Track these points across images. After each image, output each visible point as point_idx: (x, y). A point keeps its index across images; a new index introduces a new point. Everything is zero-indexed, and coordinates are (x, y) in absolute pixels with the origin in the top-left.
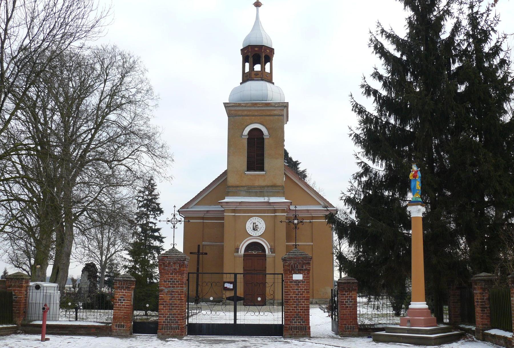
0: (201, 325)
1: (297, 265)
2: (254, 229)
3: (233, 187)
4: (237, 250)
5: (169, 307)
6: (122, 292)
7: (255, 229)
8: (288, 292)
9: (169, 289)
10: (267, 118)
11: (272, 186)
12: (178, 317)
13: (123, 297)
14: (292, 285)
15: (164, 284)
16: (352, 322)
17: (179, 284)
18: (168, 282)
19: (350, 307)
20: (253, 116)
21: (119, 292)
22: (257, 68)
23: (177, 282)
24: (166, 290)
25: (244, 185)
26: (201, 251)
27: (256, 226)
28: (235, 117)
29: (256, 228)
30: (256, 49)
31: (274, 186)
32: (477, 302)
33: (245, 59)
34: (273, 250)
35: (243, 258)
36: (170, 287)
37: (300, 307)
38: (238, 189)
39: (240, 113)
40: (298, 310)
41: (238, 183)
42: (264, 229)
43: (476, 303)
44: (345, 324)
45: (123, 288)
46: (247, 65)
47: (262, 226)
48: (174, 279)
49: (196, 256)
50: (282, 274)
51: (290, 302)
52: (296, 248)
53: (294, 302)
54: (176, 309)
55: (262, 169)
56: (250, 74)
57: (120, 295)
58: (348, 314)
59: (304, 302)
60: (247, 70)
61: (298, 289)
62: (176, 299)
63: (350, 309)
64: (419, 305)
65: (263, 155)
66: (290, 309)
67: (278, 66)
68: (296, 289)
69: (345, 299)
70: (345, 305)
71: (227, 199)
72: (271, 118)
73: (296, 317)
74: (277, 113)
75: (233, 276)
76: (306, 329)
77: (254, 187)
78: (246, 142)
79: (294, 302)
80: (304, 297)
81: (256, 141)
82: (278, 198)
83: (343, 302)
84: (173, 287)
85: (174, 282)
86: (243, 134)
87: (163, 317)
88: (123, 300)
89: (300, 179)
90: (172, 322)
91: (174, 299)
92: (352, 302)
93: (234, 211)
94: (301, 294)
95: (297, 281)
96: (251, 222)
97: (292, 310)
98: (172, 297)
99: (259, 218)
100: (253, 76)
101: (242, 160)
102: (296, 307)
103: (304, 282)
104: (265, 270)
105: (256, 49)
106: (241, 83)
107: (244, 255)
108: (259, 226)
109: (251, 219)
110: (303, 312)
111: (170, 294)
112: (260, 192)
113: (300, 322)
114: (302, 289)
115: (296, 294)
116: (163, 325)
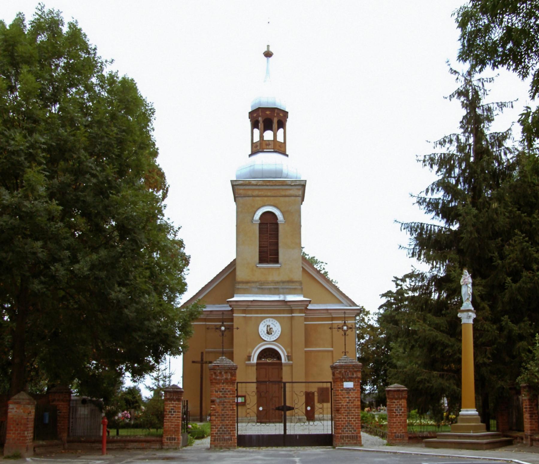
0: (250, 436)
2: (268, 333)
3: (243, 282)
4: (249, 358)
6: (173, 404)
7: (269, 333)
8: (339, 400)
10: (282, 199)
13: (173, 409)
16: (402, 430)
17: (230, 394)
18: (220, 392)
19: (400, 415)
20: (266, 196)
21: (169, 404)
22: (268, 135)
23: (229, 391)
25: (256, 280)
26: (204, 360)
27: (270, 329)
29: (270, 332)
30: (268, 112)
31: (291, 282)
32: (526, 408)
33: (255, 125)
34: (289, 358)
35: (255, 367)
36: (221, 397)
39: (250, 193)
41: (248, 278)
42: (280, 333)
43: (524, 410)
44: (396, 433)
46: (257, 132)
47: (277, 328)
48: (227, 389)
49: (199, 365)
50: (331, 382)
52: (345, 355)
54: (228, 420)
55: (276, 261)
57: (170, 407)
59: (355, 410)
60: (257, 139)
61: (349, 398)
62: (228, 410)
64: (469, 411)
65: (277, 244)
66: (341, 418)
67: (293, 132)
68: (347, 398)
70: (395, 413)
71: (235, 299)
73: (347, 426)
74: (293, 191)
76: (357, 438)
77: (267, 283)
79: (345, 410)
80: (355, 405)
81: (269, 228)
82: (295, 295)
84: (225, 397)
85: (226, 392)
86: (254, 218)
87: (216, 428)
88: (174, 412)
90: (225, 434)
93: (244, 311)
95: (348, 390)
96: (264, 324)
97: (344, 418)
98: (224, 407)
99: (274, 320)
105: (268, 112)
106: (250, 156)
107: (257, 363)
108: (274, 329)
109: (265, 320)
110: (354, 421)
112: (275, 288)
116: (215, 436)
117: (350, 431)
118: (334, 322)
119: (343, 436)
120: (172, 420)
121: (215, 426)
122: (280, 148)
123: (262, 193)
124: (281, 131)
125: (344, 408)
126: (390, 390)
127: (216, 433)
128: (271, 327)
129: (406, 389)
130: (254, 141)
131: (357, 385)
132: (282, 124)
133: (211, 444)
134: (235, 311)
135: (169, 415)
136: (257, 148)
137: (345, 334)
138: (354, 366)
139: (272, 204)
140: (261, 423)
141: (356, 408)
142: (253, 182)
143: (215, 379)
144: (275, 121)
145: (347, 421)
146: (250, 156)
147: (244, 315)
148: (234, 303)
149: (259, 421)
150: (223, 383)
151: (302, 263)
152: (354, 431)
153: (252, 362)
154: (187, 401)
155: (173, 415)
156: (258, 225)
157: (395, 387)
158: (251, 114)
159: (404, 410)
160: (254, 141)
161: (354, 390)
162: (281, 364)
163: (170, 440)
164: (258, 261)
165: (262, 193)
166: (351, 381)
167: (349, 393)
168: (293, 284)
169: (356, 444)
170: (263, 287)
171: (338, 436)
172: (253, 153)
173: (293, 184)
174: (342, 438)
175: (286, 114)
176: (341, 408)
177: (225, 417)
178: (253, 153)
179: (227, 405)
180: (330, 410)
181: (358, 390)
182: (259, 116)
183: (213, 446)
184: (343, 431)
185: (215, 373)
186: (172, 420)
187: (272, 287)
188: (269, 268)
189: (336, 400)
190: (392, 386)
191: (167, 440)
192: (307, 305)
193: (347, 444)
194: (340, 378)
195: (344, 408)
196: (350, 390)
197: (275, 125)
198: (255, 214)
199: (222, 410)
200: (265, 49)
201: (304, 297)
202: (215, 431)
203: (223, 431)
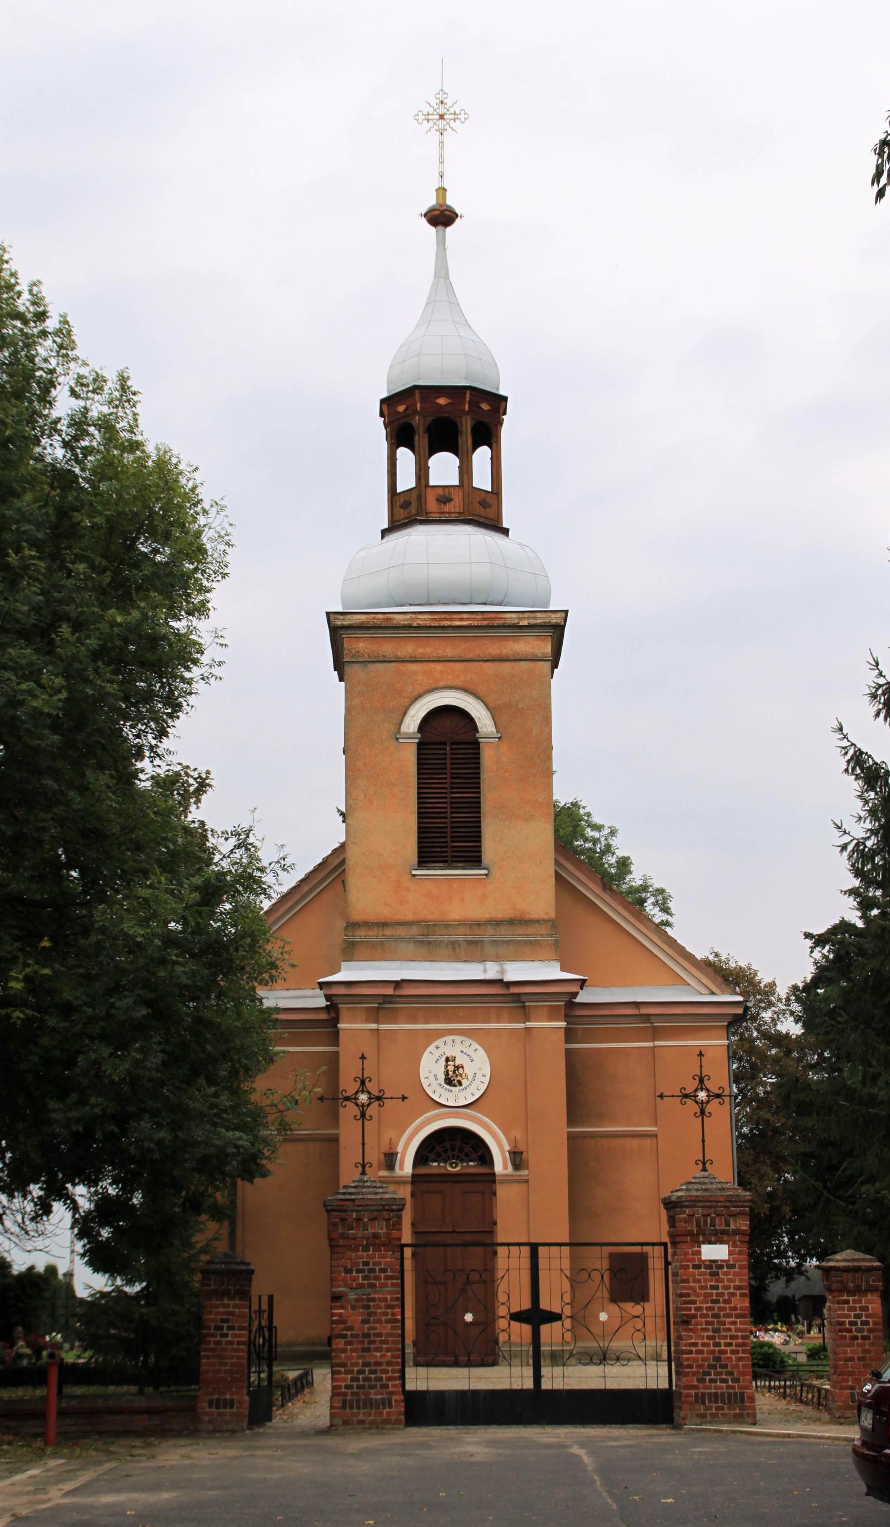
1: (713, 1219)
2: (449, 1081)
3: (368, 925)
4: (390, 1159)
5: (362, 1342)
6: (225, 1306)
8: (688, 1295)
9: (359, 1291)
11: (512, 922)
12: (387, 1372)
14: (701, 1274)
15: (345, 1279)
17: (387, 1278)
18: (358, 1271)
19: (863, 1338)
21: (217, 1306)
22: (444, 468)
23: (383, 1270)
24: (352, 1296)
25: (410, 917)
27: (457, 1068)
28: (372, 667)
29: (455, 1076)
30: (442, 401)
33: (400, 434)
34: (517, 1158)
36: (361, 1286)
37: (725, 1337)
38: (388, 932)
40: (719, 1345)
41: (384, 912)
42: (487, 1080)
44: (852, 1388)
45: (226, 1294)
47: (478, 1067)
48: (375, 1264)
50: (665, 1245)
51: (697, 1324)
53: (707, 1323)
54: (379, 1350)
56: (419, 498)
58: (859, 1359)
59: (734, 1323)
60: (406, 481)
61: (717, 1288)
62: (380, 1321)
63: (862, 1345)
65: (475, 806)
66: (695, 1344)
68: (712, 1287)
69: (849, 1316)
70: (850, 1331)
72: (506, 667)
73: (714, 1367)
75: (526, 1250)
76: (743, 1401)
77: (447, 925)
78: (409, 756)
79: (707, 1323)
80: (735, 1308)
83: (843, 1323)
84: (372, 1286)
85: (373, 1271)
86: (404, 729)
87: (346, 1372)
89: (628, 906)
90: (371, 1387)
91: (375, 1322)
92: (867, 1323)
93: (375, 1015)
94: (725, 1302)
95: (714, 1265)
97: (704, 1345)
98: (370, 1314)
99: (468, 1041)
100: (432, 505)
101: (397, 826)
102: (713, 1338)
103: (733, 1266)
104: (491, 1233)
105: (442, 401)
106: (384, 533)
107: (416, 1179)
108: (469, 1070)
110: (732, 1352)
111: (364, 1307)
112: (470, 943)
113: (726, 1381)
114: (728, 1288)
115: (713, 1301)
116: (345, 1394)
117: (723, 1381)
118: (657, 1043)
119: (703, 1394)
120: (226, 1350)
121: (344, 1365)
122: (482, 511)
123: (428, 650)
124: (482, 456)
125: (703, 1316)
126: (831, 1267)
127: (347, 1387)
128: (457, 1063)
129: (878, 1264)
130: (400, 489)
131: (740, 1253)
132: (487, 433)
133: (332, 1416)
134: (344, 1014)
135: (215, 1336)
136: (409, 510)
137: (703, 1112)
138: (729, 1199)
139: (458, 683)
140: (428, 1364)
141: (737, 1316)
142: (396, 616)
143: (344, 1237)
144: (466, 425)
145: (713, 1352)
146: (384, 533)
147: (374, 1026)
148: (342, 991)
149: (421, 1359)
150: (366, 1249)
151: (557, 862)
152: (734, 1380)
153: (398, 1172)
154: (271, 1298)
155: (226, 1335)
156: (415, 747)
157: (846, 1260)
158: (388, 404)
159: (875, 1323)
160: (400, 489)
161: (730, 1266)
162: (491, 1178)
163: (218, 1407)
164: (414, 859)
165: (428, 650)
166: (722, 1242)
167: (717, 1274)
168: (530, 931)
169: (739, 1418)
170: (432, 938)
171: (688, 1395)
172: (395, 525)
173: (525, 623)
174: (700, 1399)
175: (498, 403)
176: (695, 1316)
177: (370, 1342)
178: (395, 525)
179: (378, 1307)
180: (661, 1322)
181: (741, 1267)
182: (416, 412)
183: (338, 1421)
184: (704, 1381)
185: (343, 1220)
186: (226, 1350)
187: (461, 938)
188: (449, 880)
189: (681, 1295)
190: (838, 1257)
191: (210, 1406)
192: (575, 994)
193: (714, 1418)
194: (690, 1233)
195: (703, 1316)
196: (721, 1267)
197: (466, 438)
198: (405, 714)
199: (365, 1322)
200: (431, 201)
201: (563, 969)
202: (345, 1380)
203: (366, 1379)
